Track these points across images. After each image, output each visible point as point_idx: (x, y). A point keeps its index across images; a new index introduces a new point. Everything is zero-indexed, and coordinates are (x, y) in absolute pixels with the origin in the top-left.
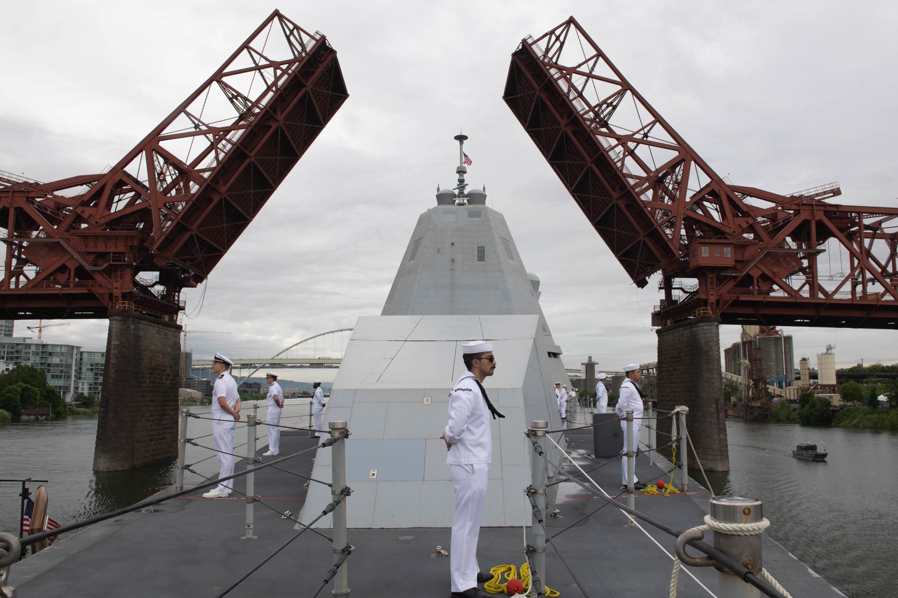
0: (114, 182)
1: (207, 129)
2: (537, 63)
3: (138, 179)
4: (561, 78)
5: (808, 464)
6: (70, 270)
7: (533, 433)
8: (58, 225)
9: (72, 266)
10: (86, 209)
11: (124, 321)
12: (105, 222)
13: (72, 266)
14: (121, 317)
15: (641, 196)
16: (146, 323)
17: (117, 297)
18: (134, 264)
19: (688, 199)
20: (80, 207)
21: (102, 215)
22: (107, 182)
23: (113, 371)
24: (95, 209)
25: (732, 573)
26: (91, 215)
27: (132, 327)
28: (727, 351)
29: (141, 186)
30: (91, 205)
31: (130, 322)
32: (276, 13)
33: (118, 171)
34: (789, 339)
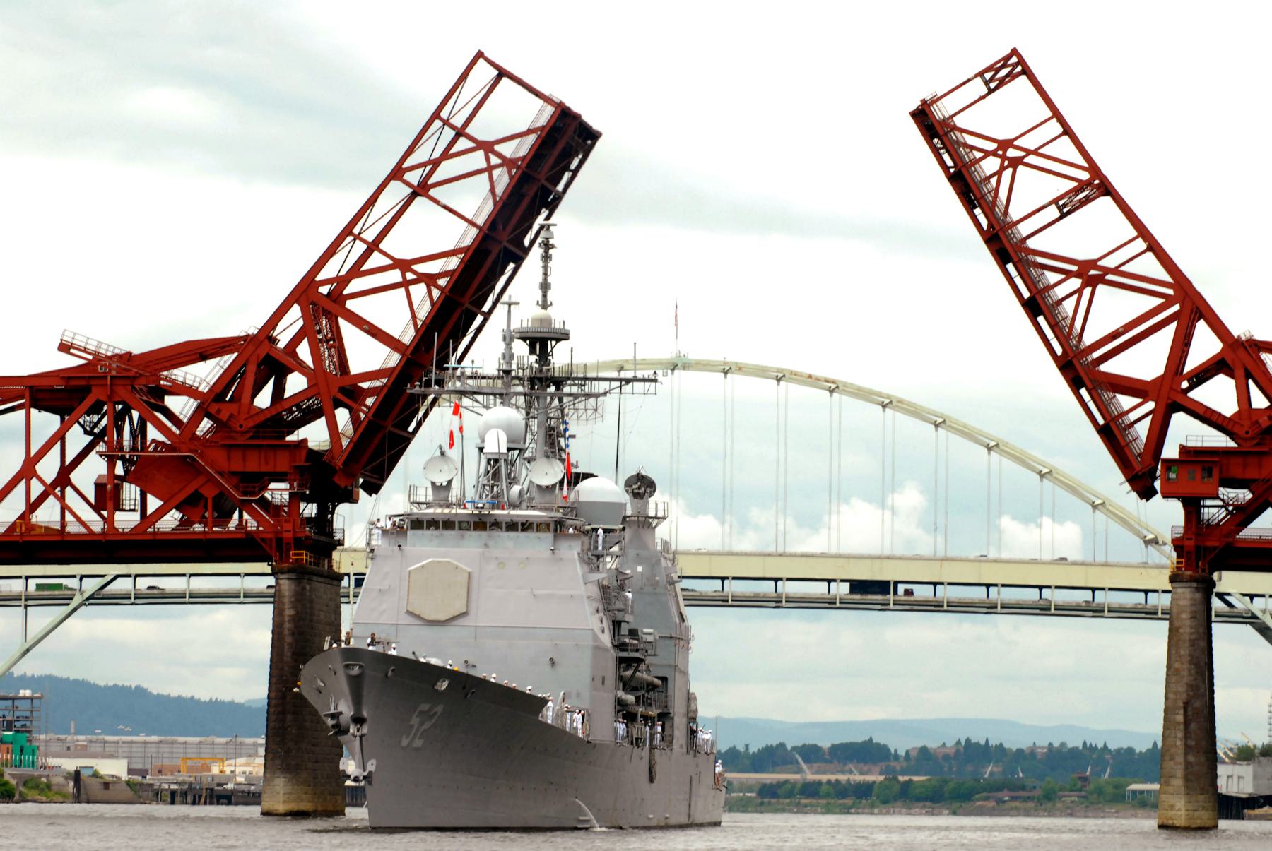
0: (258, 359)
1: (306, 340)
2: (470, 260)
3: (300, 315)
4: (439, 290)
5: (1120, 605)
6: (206, 499)
7: (492, 462)
8: (592, 140)
9: (209, 493)
10: (222, 406)
11: (298, 581)
12: (253, 424)
13: (209, 493)
14: (294, 574)
15: (406, 343)
16: (320, 579)
17: (287, 544)
18: (307, 492)
19: (236, 354)
20: (213, 404)
21: (248, 413)
22: (248, 360)
23: (289, 654)
24: (235, 407)
25: (348, 387)
26: (231, 415)
27: (308, 587)
28: (1156, 493)
29: (955, 830)
30: (227, 399)
31: (306, 581)
32: (480, 55)
33: (262, 342)
34: (1184, 450)
